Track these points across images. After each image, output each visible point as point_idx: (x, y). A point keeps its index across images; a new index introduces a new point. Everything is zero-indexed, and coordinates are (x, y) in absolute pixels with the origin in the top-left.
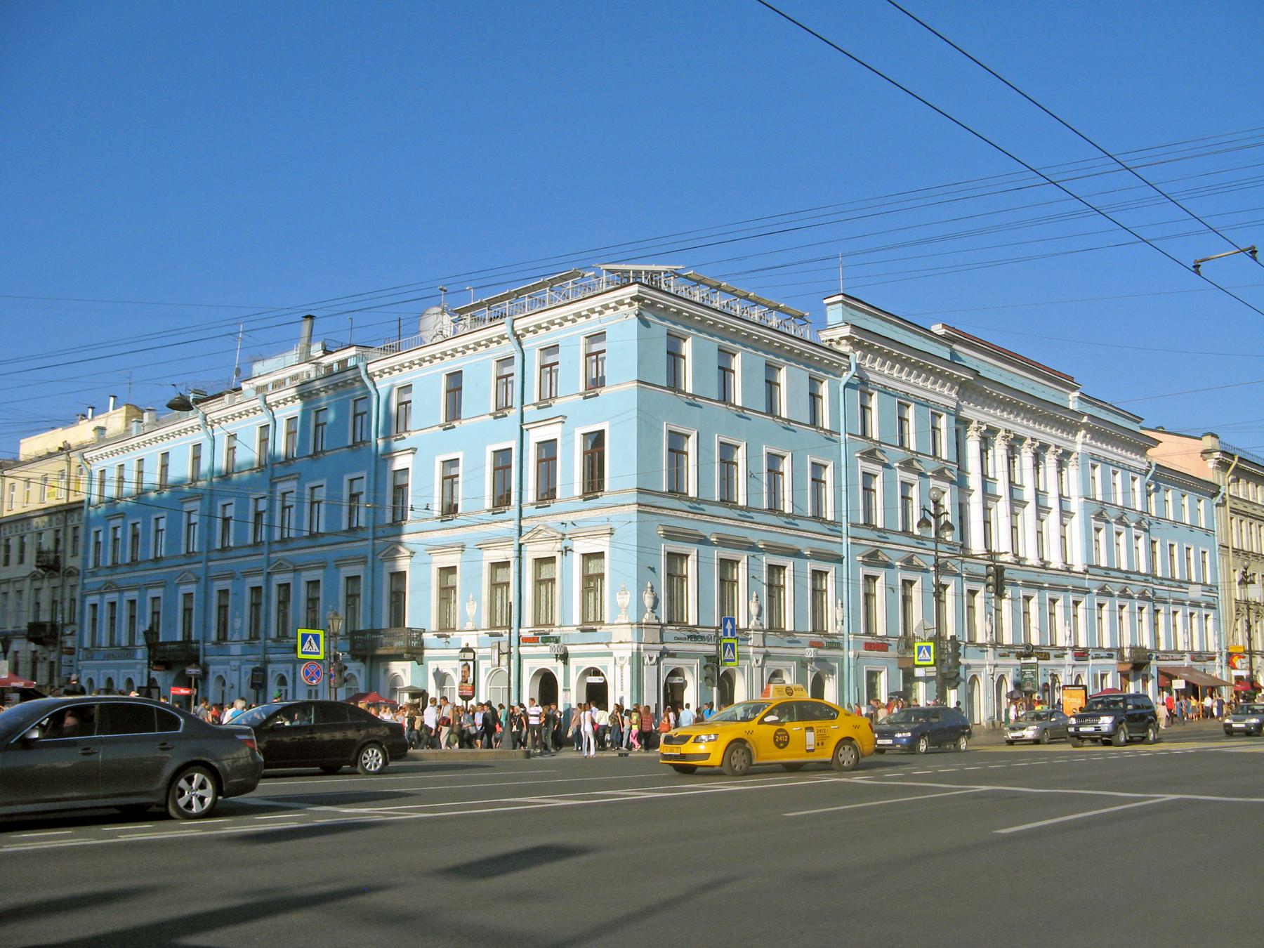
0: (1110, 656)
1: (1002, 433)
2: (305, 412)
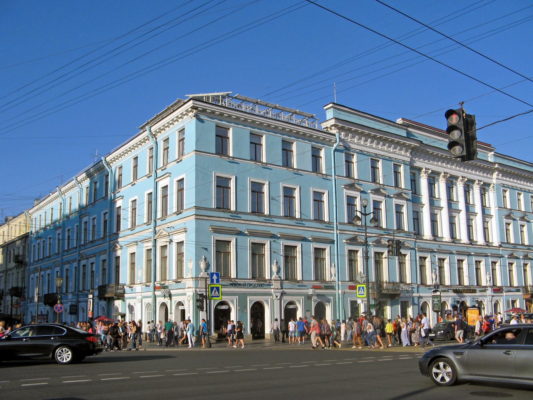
0: (518, 291)
1: (443, 174)
2: (91, 183)
